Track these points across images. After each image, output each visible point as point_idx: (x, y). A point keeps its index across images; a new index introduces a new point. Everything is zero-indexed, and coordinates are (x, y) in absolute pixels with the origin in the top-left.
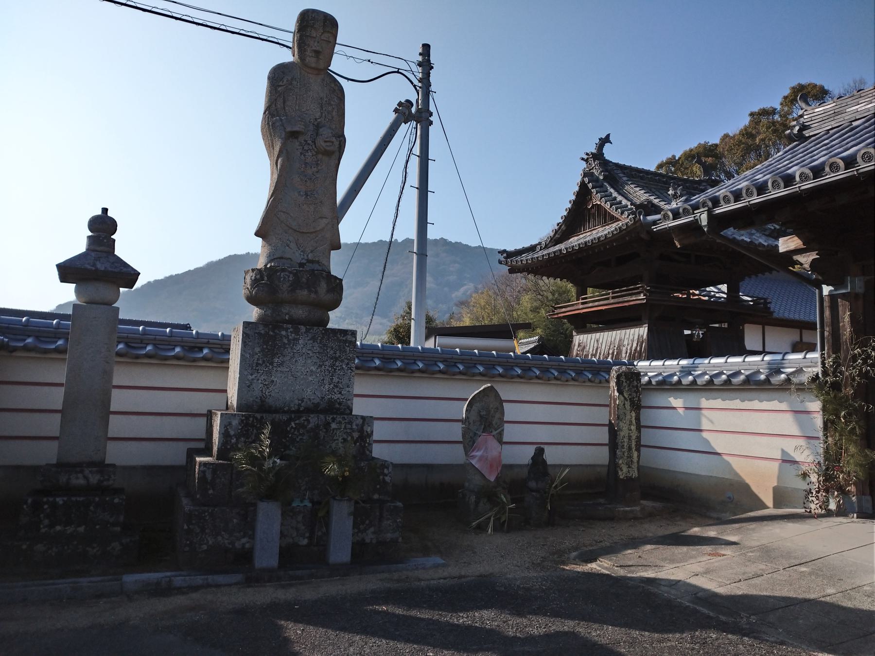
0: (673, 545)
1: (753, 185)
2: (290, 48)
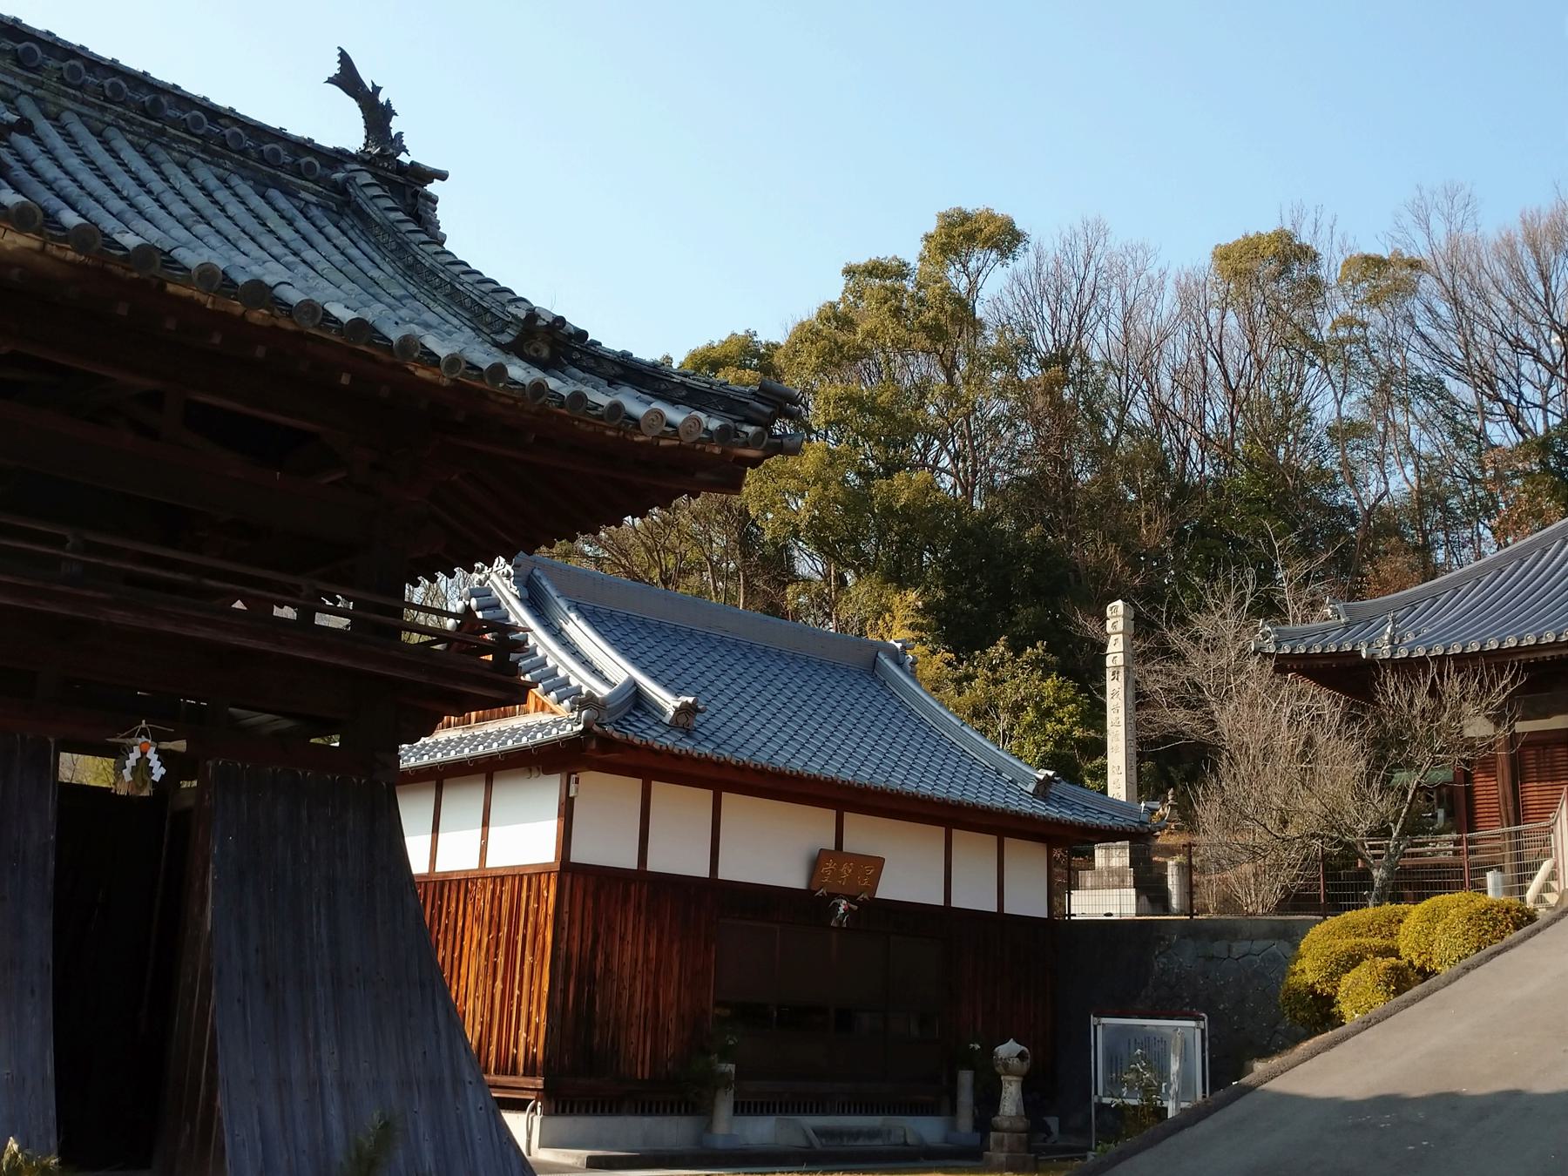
2: (490, 1087)
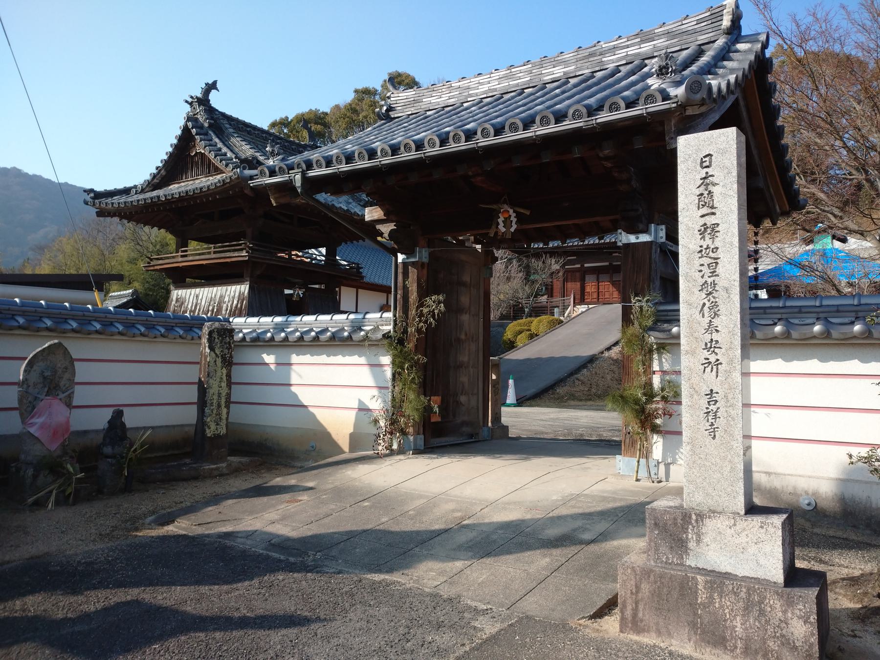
0: (256, 497)
1: (343, 153)
